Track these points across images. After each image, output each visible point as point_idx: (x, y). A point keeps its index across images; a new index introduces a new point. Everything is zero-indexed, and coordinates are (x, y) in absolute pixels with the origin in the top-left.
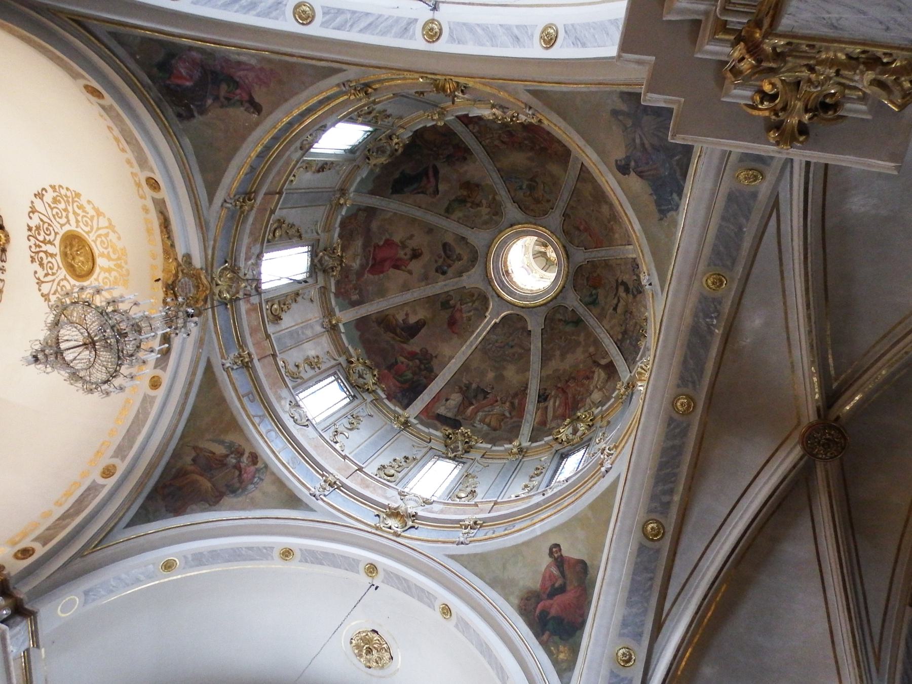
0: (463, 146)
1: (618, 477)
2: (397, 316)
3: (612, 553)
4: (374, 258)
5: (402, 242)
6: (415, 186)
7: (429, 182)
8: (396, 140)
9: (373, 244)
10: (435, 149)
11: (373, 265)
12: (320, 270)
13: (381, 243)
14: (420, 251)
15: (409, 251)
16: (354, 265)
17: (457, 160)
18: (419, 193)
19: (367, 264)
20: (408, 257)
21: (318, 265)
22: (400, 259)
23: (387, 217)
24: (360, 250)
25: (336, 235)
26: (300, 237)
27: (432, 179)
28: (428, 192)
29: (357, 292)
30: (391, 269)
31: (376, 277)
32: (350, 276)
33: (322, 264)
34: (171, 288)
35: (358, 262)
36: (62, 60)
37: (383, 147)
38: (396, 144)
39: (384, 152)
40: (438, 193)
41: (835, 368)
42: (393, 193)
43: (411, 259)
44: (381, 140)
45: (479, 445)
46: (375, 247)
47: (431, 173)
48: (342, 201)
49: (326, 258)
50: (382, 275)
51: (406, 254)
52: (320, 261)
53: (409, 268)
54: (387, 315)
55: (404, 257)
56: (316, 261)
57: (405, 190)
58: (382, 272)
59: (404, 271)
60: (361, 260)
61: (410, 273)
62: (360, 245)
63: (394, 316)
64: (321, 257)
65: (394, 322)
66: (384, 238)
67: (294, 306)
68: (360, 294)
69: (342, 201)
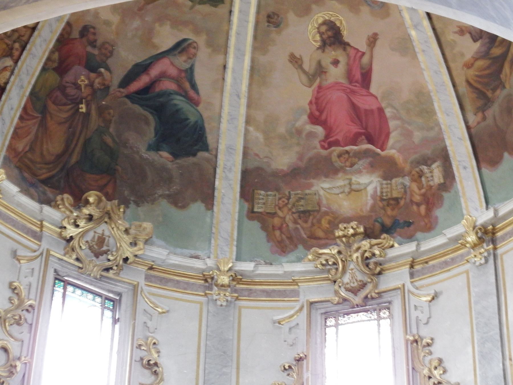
0: (56, 56)
1: (339, 17)
2: (468, 56)
3: (305, 286)
4: (354, 141)
5: (311, 78)
6: (179, 101)
7: (163, 75)
9: (324, 152)
10: (83, 108)
11: (370, 140)
13: (319, 130)
14: (323, 28)
15: (333, 53)
16: (370, 189)
17: (93, 44)
18: (194, 86)
19: (366, 153)
20: (339, 54)
21: (363, 294)
22: (349, 75)
23: (260, 136)
24: (340, 181)
25: (299, 267)
27: (154, 72)
28: (187, 66)
29: (425, 168)
30: (373, 89)
31: (392, 124)
32: (395, 195)
37: (90, 248)
38: (77, 226)
39: (101, 240)
40: (185, 40)
42: (206, 148)
43: (345, 45)
44: (78, 259)
45: (391, 253)
46: (331, 145)
47: (144, 80)
49: (347, 279)
50: (388, 112)
51: (336, 63)
53: (363, 47)
54: (468, 82)
55: (342, 67)
56: (357, 300)
57: (192, 119)
58: (381, 110)
59: (372, 57)
60: (359, 172)
61: (373, 40)
62: (326, 185)
63: (468, 66)
64: (347, 290)
65: (480, 63)
66: (310, 127)
68: (427, 161)
69: (225, 280)
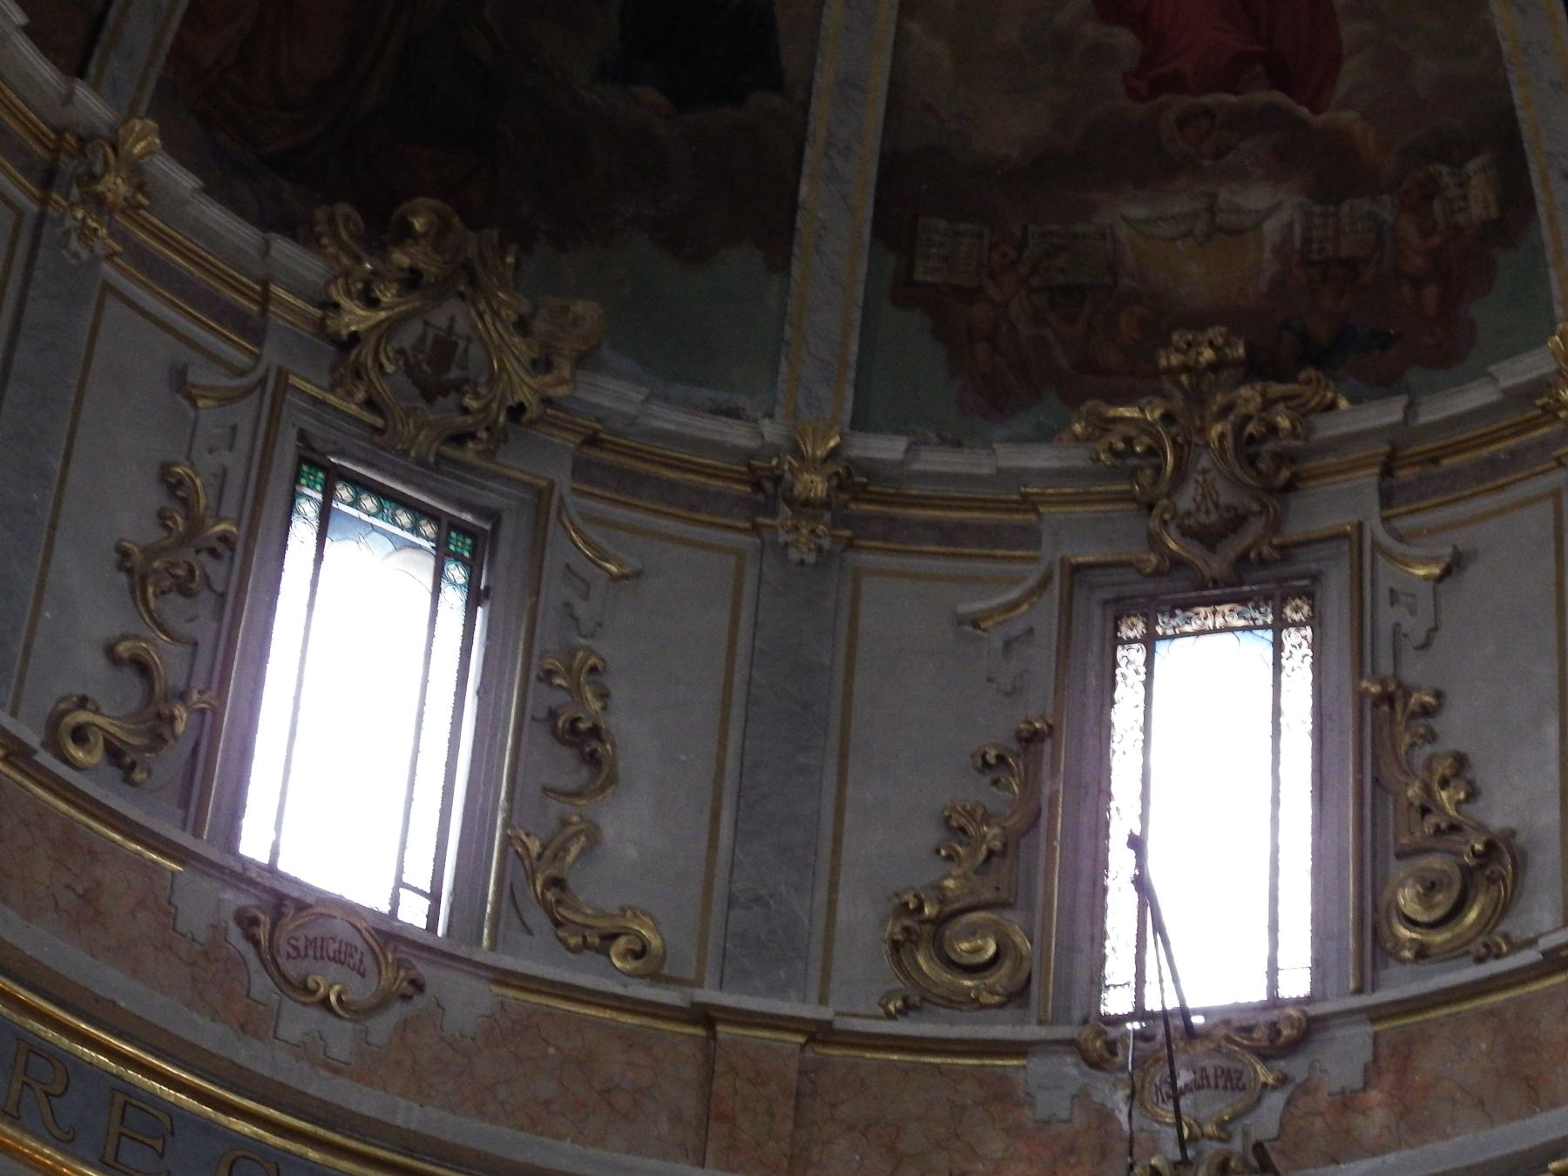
8: (355, 317)
12: (1275, 526)
13: (1125, 39)
25: (1042, 458)
26: (1031, 739)
33: (1236, 521)
34: (1343, 1092)
35: (1255, 198)
36: (409, 1152)
37: (410, 371)
38: (372, 303)
39: (444, 348)
41: (1052, 1015)
44: (370, 404)
48: (816, 485)
49: (1187, 499)
52: (1208, 538)
56: (1216, 565)
62: (1137, 211)
64: (1186, 532)
67: (1455, 730)
69: (816, 485)
